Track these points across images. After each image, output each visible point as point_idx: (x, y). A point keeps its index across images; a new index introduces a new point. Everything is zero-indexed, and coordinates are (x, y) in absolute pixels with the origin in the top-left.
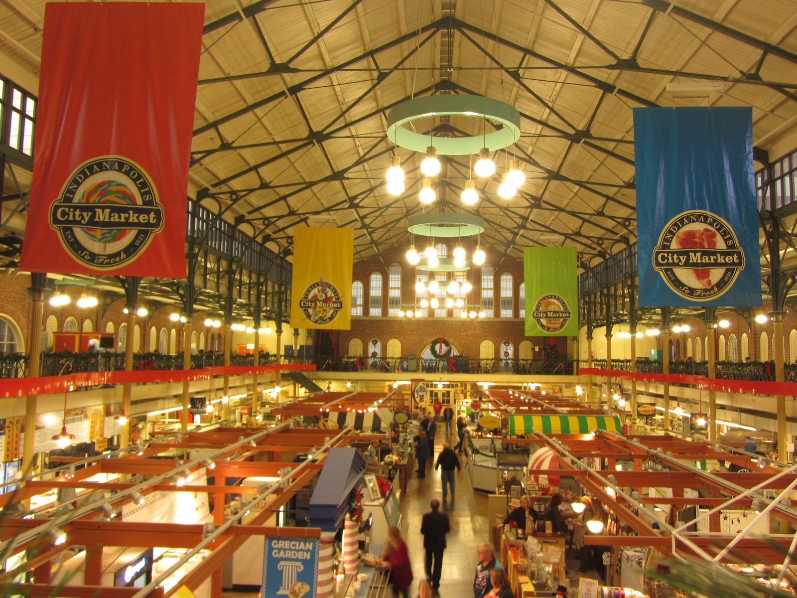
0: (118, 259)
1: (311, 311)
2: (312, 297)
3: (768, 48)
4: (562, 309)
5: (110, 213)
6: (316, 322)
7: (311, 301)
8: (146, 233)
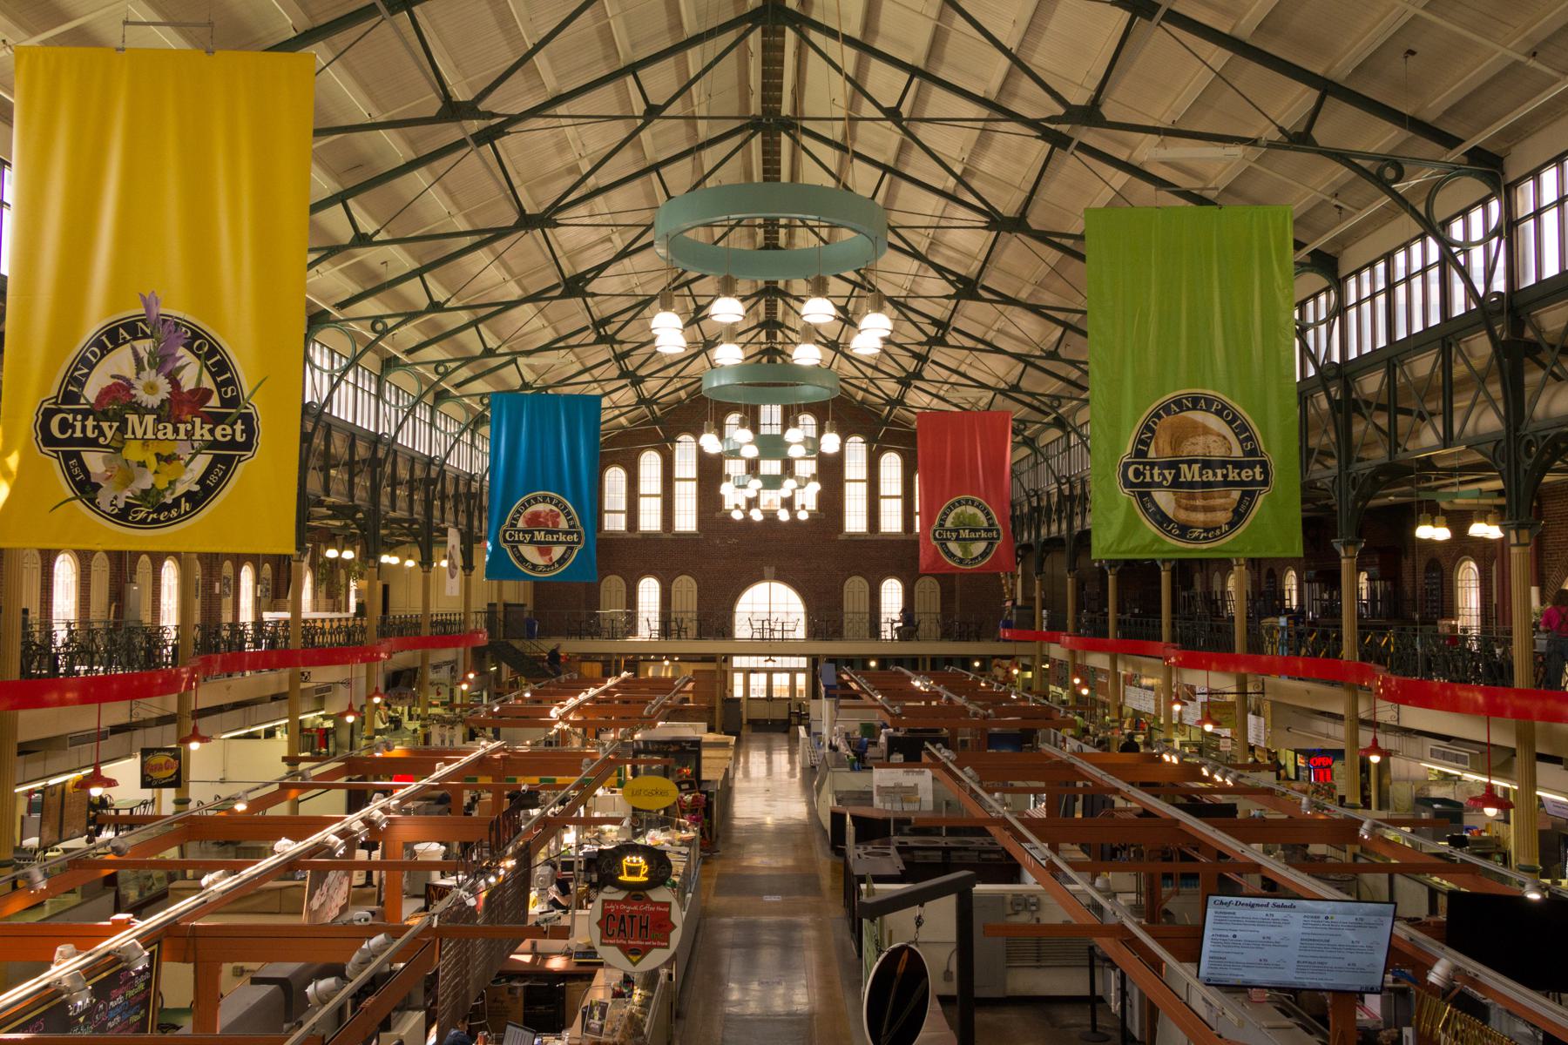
0: (174, 513)
1: (95, 461)
2: (106, 393)
3: (1327, 88)
4: (1237, 452)
5: (1201, 470)
6: (123, 516)
7: (98, 412)
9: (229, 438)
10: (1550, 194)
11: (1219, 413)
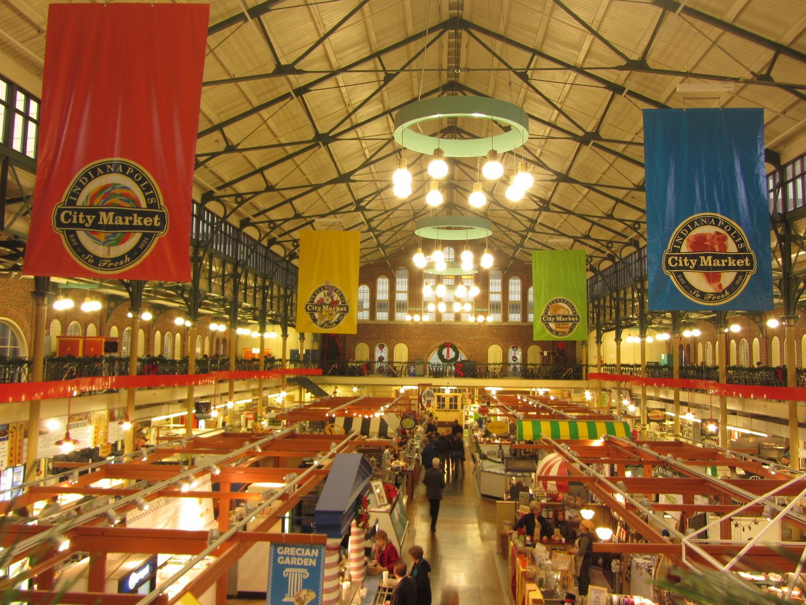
0: (122, 263)
1: (317, 315)
2: (319, 301)
3: (779, 49)
4: (571, 313)
5: (114, 216)
6: (322, 326)
7: (317, 305)
8: (150, 236)
9: (150, 224)
10: (798, 171)
11: (566, 303)
